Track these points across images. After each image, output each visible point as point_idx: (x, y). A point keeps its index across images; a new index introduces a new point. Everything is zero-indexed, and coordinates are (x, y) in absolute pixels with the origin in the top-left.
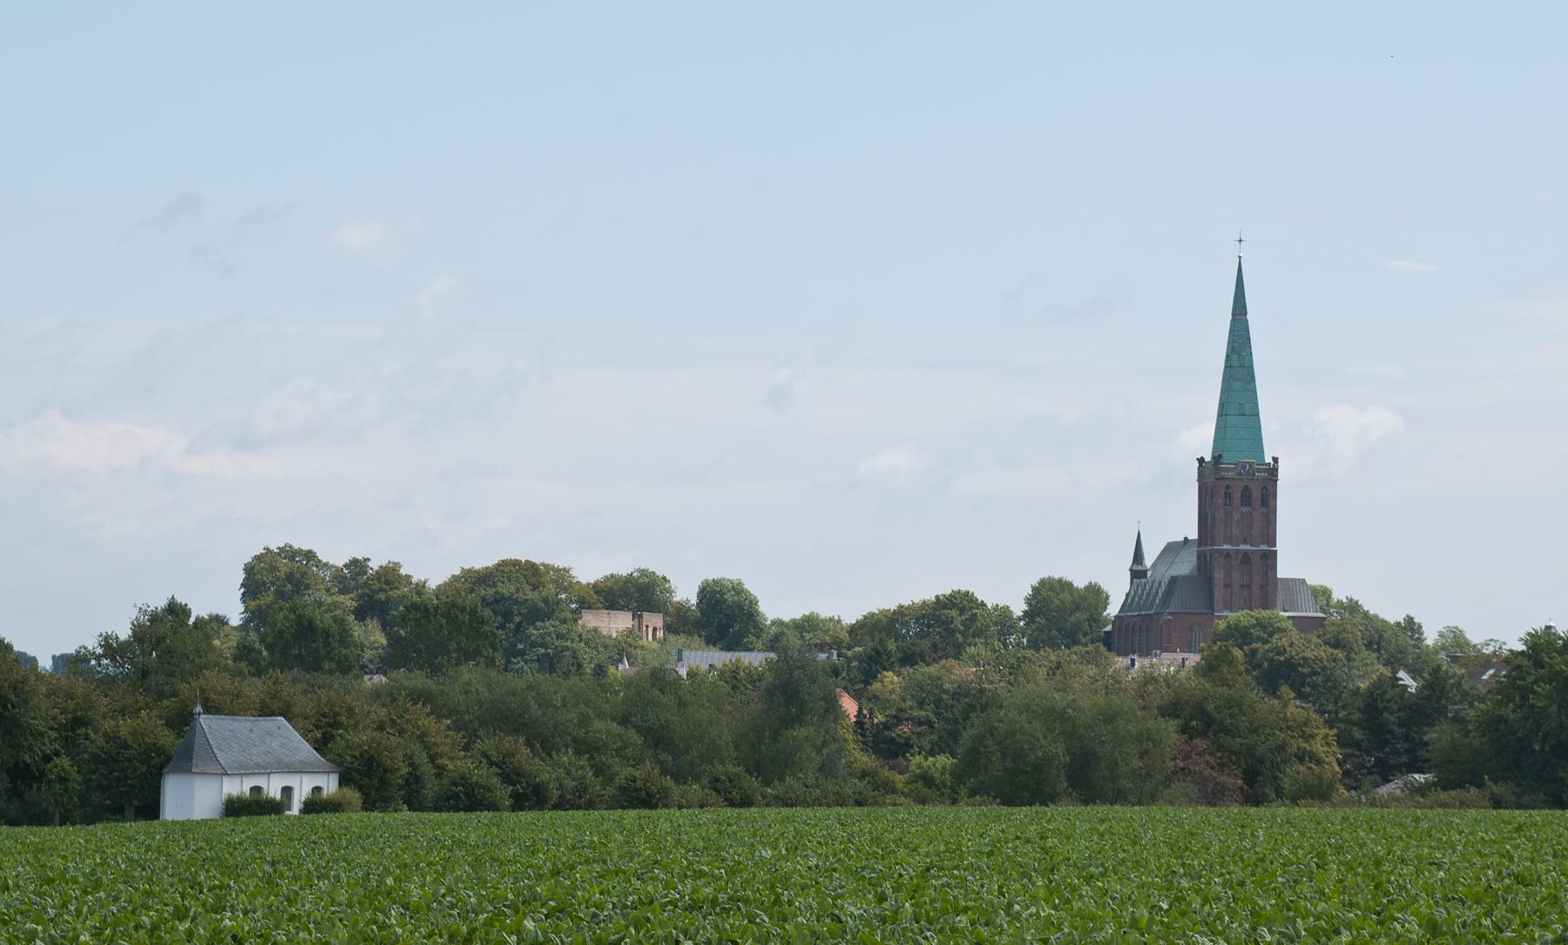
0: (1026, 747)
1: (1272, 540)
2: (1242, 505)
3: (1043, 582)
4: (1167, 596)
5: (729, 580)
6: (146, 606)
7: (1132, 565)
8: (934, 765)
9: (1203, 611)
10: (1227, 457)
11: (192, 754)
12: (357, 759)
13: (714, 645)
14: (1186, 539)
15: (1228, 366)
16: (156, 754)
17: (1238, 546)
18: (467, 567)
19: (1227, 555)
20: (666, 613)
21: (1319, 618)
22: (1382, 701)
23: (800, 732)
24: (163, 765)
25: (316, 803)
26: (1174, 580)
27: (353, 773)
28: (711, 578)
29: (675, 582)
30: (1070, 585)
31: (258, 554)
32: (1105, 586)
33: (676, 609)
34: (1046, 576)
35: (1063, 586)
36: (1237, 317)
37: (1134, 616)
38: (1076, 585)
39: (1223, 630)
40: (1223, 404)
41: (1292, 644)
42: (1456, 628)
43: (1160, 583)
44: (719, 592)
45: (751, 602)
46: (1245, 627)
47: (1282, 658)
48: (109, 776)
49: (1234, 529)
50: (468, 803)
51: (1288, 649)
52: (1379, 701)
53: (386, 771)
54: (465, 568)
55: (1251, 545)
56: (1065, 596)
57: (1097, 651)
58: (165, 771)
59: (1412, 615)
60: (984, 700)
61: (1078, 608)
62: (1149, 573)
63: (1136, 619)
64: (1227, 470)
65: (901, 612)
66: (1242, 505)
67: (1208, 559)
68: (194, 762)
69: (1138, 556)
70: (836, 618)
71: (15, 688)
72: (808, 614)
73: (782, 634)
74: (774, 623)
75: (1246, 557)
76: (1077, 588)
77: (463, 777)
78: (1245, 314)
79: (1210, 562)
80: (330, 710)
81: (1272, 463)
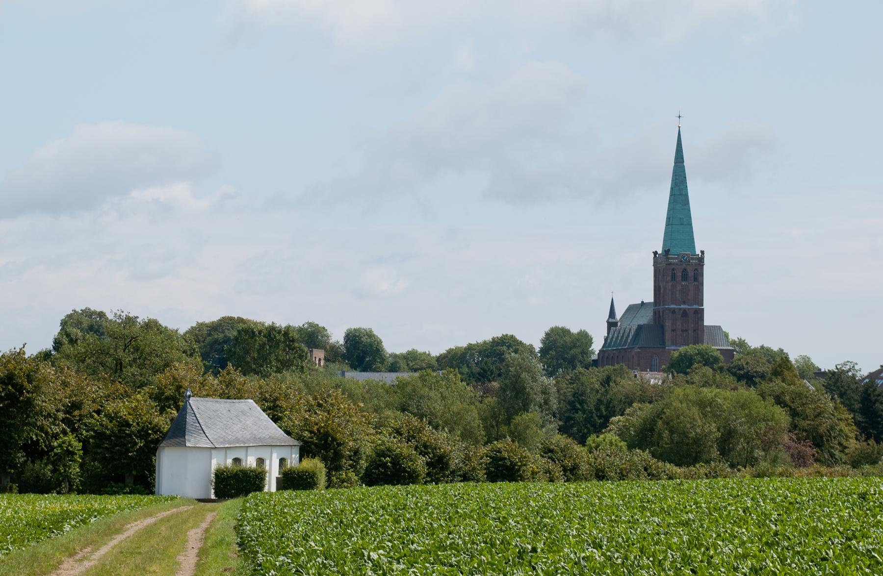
0: (688, 426)
1: (699, 298)
2: (682, 280)
3: (552, 330)
4: (636, 337)
5: (364, 329)
7: (609, 319)
8: (604, 441)
9: (659, 346)
10: (672, 251)
11: (185, 431)
12: (315, 434)
13: (356, 369)
14: (642, 302)
16: (153, 431)
17: (680, 305)
18: (200, 321)
19: (673, 311)
20: (325, 349)
21: (730, 350)
22: (874, 396)
23: (527, 416)
24: (157, 442)
25: (294, 472)
26: (640, 328)
27: (313, 446)
29: (330, 331)
30: (568, 331)
31: (69, 313)
32: (590, 332)
33: (330, 347)
34: (554, 326)
35: (565, 332)
36: (678, 164)
37: (614, 350)
38: (572, 332)
39: (677, 357)
40: (669, 218)
41: (747, 363)
43: (630, 330)
44: (358, 336)
45: (378, 343)
46: (691, 355)
47: (742, 372)
49: (677, 296)
50: (394, 470)
51: (745, 366)
52: (872, 396)
53: (339, 445)
54: (199, 322)
55: (688, 305)
56: (567, 339)
57: (621, 369)
58: (161, 445)
59: (783, 348)
60: (608, 396)
61: (574, 346)
63: (614, 352)
65: (470, 348)
66: (682, 280)
67: (661, 314)
68: (186, 437)
70: (427, 353)
72: (410, 350)
73: (396, 362)
74: (391, 355)
75: (685, 313)
76: (573, 334)
77: (389, 450)
78: (683, 162)
79: (663, 316)
80: (270, 396)
81: (700, 254)
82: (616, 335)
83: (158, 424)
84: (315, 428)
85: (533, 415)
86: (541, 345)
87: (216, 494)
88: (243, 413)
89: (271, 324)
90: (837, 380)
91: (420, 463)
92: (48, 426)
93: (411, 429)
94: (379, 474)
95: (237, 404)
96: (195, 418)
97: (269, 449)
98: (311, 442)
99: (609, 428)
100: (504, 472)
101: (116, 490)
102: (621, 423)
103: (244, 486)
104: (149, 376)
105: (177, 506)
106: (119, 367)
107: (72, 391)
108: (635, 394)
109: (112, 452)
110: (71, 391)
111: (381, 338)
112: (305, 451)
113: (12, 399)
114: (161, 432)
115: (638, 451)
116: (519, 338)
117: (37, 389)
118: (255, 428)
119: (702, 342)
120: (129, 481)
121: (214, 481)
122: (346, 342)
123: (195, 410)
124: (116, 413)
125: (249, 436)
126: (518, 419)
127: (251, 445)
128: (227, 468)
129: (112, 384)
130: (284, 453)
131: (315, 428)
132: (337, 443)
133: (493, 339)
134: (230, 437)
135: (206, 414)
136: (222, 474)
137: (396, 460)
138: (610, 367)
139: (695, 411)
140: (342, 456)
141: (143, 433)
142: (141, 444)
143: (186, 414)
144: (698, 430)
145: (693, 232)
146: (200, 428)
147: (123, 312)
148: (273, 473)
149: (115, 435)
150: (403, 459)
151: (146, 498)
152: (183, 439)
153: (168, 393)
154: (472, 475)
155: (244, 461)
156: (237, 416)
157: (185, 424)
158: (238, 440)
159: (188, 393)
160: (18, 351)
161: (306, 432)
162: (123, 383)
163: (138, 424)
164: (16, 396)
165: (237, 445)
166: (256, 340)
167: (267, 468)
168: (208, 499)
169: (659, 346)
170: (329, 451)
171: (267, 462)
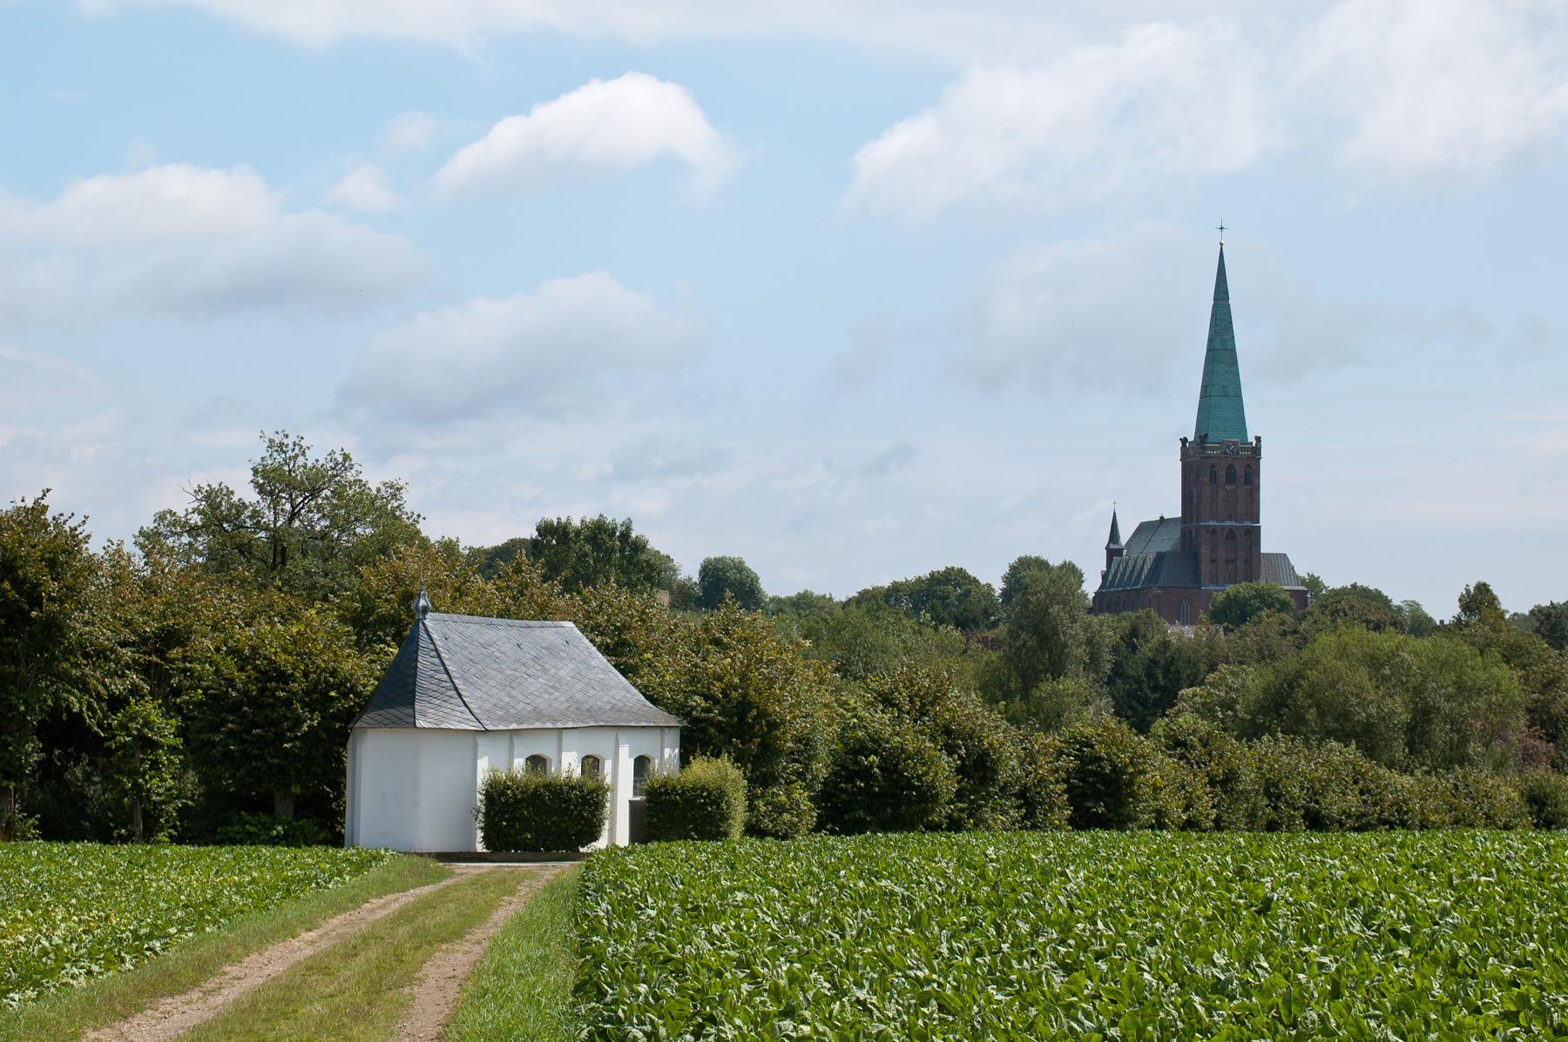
1: (1254, 515)
6: (281, 435)
9: (1191, 585)
12: (717, 702)
14: (1162, 518)
15: (1210, 349)
19: (1213, 531)
24: (349, 716)
26: (1160, 557)
27: (712, 730)
28: (713, 557)
32: (1079, 565)
34: (1023, 555)
35: (1041, 564)
42: (1413, 601)
44: (721, 570)
48: (245, 736)
53: (773, 726)
55: (1236, 521)
57: (1149, 617)
58: (358, 724)
60: (1168, 654)
62: (1125, 552)
64: (1212, 449)
68: (417, 706)
69: (1114, 535)
70: (828, 596)
71: (52, 564)
74: (773, 600)
75: (1231, 534)
76: (1053, 568)
82: (1121, 569)
83: (352, 675)
84: (716, 689)
85: (1070, 684)
86: (1002, 585)
87: (487, 840)
88: (551, 650)
89: (596, 518)
90: (1554, 626)
91: (943, 772)
92: (97, 679)
93: (916, 695)
94: (854, 794)
95: (537, 632)
96: (437, 661)
97: (610, 736)
98: (705, 720)
99: (1176, 708)
100: (1099, 786)
101: (252, 829)
102: (1197, 699)
103: (553, 823)
104: (343, 576)
105: (385, 887)
106: (279, 559)
107: (168, 604)
108: (1198, 651)
109: (243, 741)
110: (164, 604)
111: (756, 572)
112: (694, 742)
113: (16, 617)
114: (358, 695)
115: (1334, 744)
116: (972, 572)
117: (71, 591)
118: (579, 686)
119: (1258, 578)
120: (284, 809)
121: (483, 809)
122: (703, 579)
123: (437, 642)
124: (254, 649)
125: (565, 705)
126: (1046, 687)
127: (570, 725)
128: (513, 779)
129: (261, 592)
130: (647, 744)
131: (716, 689)
132: (768, 722)
133: (932, 575)
134: (520, 706)
135: (465, 653)
136: (503, 794)
137: (893, 764)
138: (1130, 613)
139: (1362, 676)
140: (778, 752)
141: (317, 697)
142: (312, 721)
143: (416, 652)
144: (1373, 710)
145: (1243, 408)
146: (449, 684)
147: (287, 436)
148: (623, 794)
149: (253, 702)
150: (905, 761)
151: (311, 857)
152: (409, 711)
153: (384, 609)
154: (1038, 793)
155: (554, 763)
156: (536, 659)
157: (415, 675)
158: (538, 714)
159: (422, 603)
160: (30, 505)
161: (696, 698)
162: (285, 589)
163: (305, 675)
164: (21, 610)
165: (538, 725)
166: (570, 548)
167: (608, 780)
168: (469, 853)
169: (1191, 585)
170: (750, 740)
171: (608, 766)
